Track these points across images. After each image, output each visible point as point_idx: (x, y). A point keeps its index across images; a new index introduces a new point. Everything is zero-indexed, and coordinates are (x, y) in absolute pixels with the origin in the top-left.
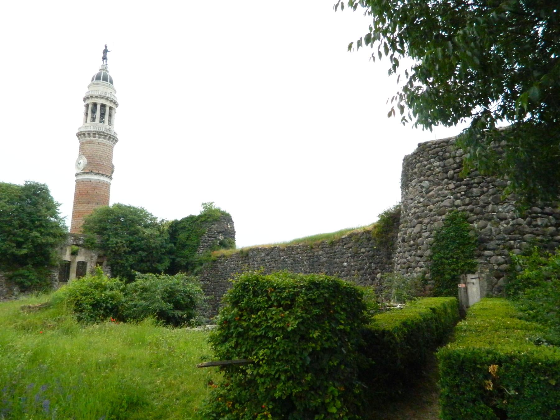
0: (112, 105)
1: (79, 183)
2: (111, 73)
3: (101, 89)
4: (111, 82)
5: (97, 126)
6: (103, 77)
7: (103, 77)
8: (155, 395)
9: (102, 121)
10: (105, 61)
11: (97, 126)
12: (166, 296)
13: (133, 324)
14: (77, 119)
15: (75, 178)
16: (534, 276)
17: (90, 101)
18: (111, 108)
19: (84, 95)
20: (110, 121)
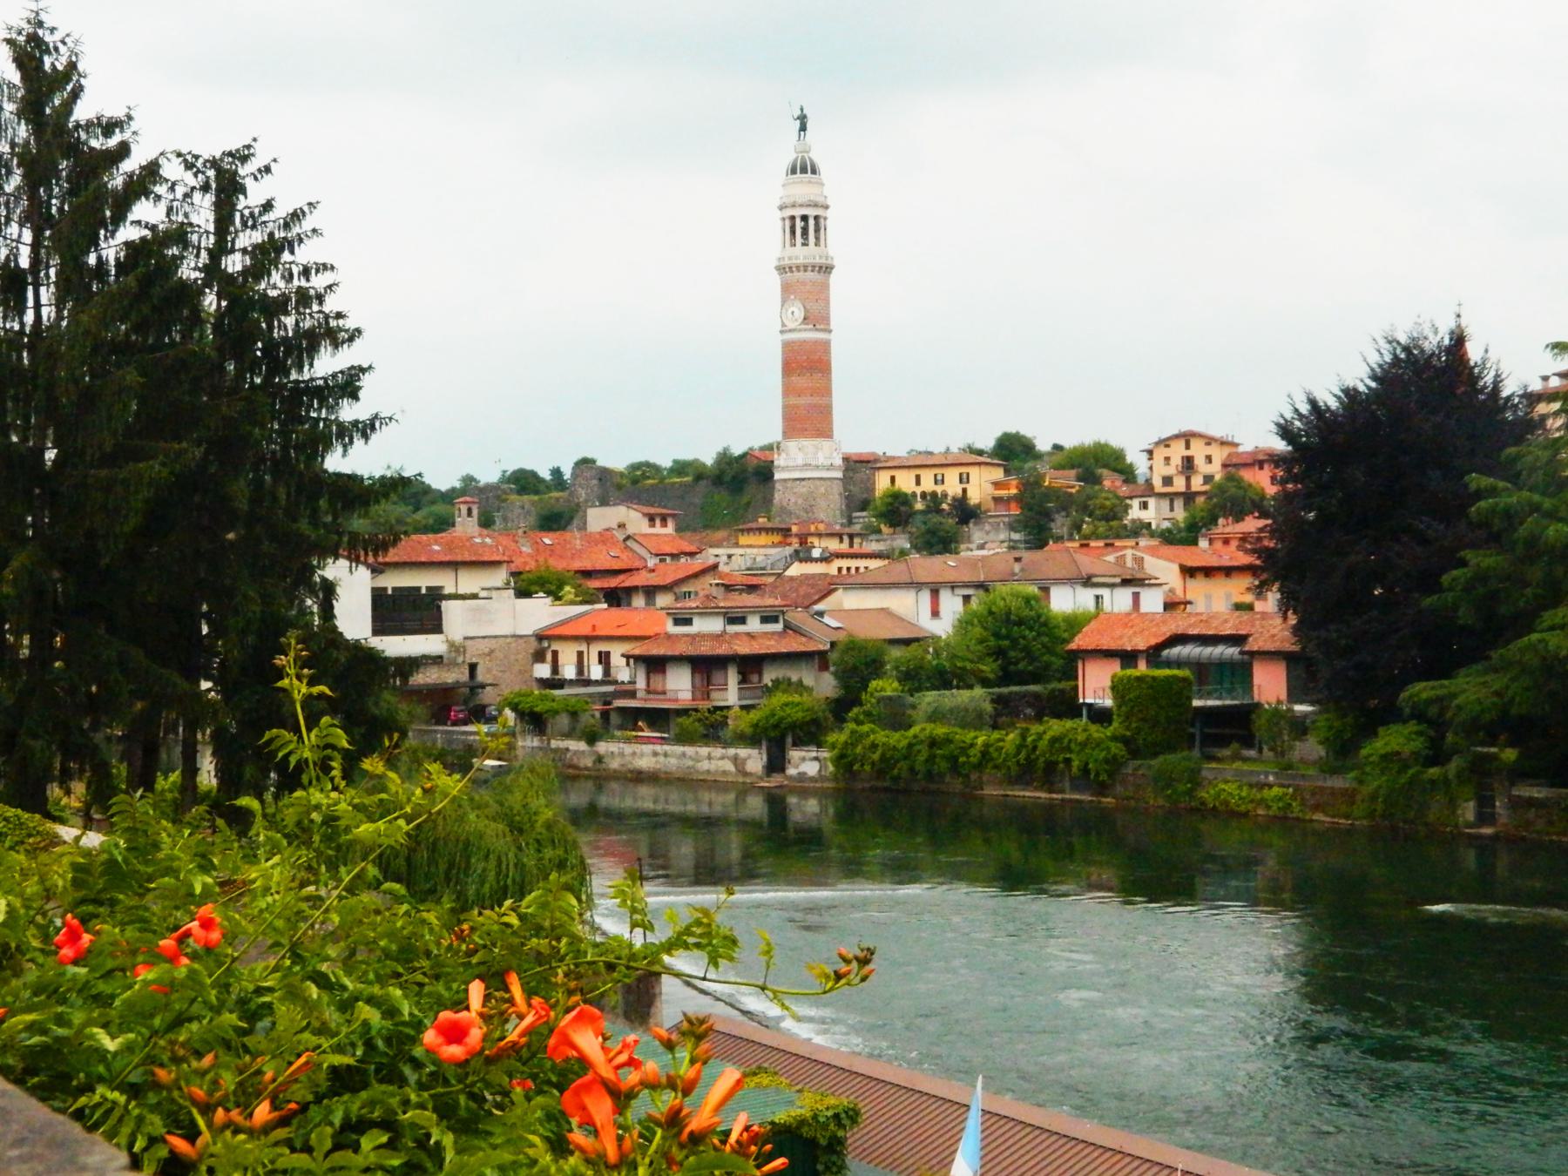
1: (786, 407)
2: (816, 156)
3: (802, 189)
5: (801, 254)
6: (804, 168)
7: (804, 168)
11: (801, 254)
12: (1068, 521)
14: (771, 244)
15: (779, 214)
16: (1221, 521)
17: (789, 212)
18: (816, 218)
19: (778, 203)
20: (817, 238)
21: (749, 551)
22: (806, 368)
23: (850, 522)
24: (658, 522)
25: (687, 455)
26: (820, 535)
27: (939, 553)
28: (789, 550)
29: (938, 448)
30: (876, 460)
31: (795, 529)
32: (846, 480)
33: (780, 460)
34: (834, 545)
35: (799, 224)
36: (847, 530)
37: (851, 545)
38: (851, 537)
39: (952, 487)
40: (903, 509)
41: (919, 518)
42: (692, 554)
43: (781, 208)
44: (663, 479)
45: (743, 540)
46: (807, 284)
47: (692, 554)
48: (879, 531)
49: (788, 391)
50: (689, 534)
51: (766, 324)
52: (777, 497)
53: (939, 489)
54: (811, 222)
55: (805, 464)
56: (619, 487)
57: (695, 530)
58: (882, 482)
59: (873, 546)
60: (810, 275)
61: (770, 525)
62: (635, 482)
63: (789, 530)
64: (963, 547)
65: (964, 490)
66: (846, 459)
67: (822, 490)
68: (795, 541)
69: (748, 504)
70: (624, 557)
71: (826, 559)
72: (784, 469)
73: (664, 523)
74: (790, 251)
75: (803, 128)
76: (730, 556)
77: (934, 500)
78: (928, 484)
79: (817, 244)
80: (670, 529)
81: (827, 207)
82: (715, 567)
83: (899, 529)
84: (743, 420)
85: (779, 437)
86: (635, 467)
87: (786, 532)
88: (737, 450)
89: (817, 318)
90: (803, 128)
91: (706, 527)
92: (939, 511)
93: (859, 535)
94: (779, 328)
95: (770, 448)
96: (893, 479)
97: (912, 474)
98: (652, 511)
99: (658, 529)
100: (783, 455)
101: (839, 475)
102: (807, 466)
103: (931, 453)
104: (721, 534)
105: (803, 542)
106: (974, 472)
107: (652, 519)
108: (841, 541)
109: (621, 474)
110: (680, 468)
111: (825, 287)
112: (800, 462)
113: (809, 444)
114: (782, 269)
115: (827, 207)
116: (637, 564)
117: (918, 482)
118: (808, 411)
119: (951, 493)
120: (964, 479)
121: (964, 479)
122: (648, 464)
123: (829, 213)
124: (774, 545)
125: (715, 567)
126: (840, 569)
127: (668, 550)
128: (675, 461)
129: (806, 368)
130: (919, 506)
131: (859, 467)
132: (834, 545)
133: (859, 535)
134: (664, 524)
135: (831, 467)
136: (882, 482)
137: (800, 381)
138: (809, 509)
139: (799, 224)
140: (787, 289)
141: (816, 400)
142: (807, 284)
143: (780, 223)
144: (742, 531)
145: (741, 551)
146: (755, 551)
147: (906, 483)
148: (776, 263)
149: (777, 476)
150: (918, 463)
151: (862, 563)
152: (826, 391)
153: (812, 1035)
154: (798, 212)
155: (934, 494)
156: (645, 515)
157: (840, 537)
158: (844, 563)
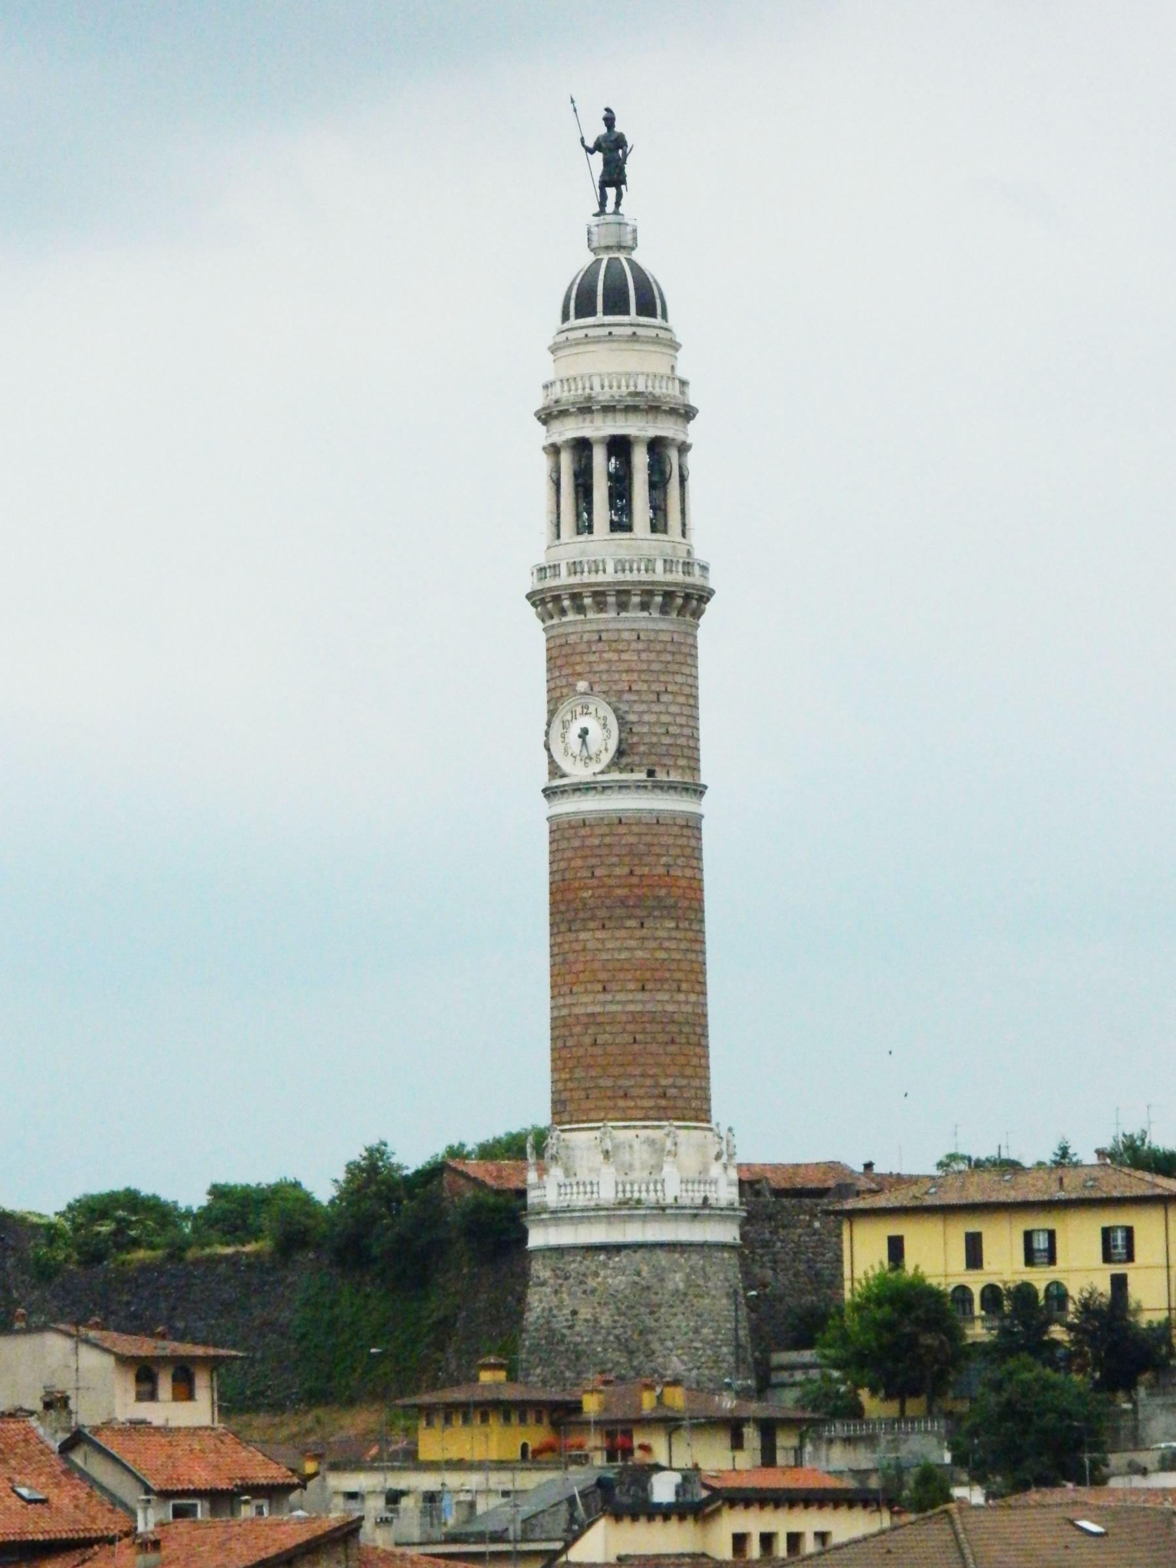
0: (664, 428)
2: (648, 257)
3: (612, 363)
4: (649, 303)
5: (606, 554)
6: (615, 294)
7: (615, 294)
8: (620, 1188)
9: (622, 525)
10: (611, 192)
11: (606, 554)
13: (872, 1268)
14: (515, 520)
15: (541, 436)
17: (571, 429)
20: (659, 510)
21: (453, 1480)
22: (627, 910)
23: (764, 1386)
24: (165, 1386)
25: (254, 1171)
26: (670, 1424)
27: (1046, 1481)
28: (579, 1478)
29: (1033, 1150)
30: (845, 1189)
31: (591, 1405)
32: (748, 1250)
33: (546, 1189)
34: (715, 1459)
35: (601, 464)
36: (754, 1408)
37: (768, 1458)
38: (768, 1429)
39: (1080, 1268)
40: (928, 1340)
41: (978, 1372)
42: (275, 1493)
43: (547, 417)
44: (177, 1251)
45: (433, 1443)
46: (627, 642)
47: (275, 1493)
48: (855, 1412)
49: (565, 974)
50: (261, 1420)
51: (486, 765)
52: (537, 1301)
53: (1040, 1279)
54: (640, 458)
55: (596, 1188)
56: (45, 1272)
57: (277, 1407)
58: (864, 1255)
59: (833, 1462)
60: (635, 618)
61: (512, 1393)
62: (93, 1256)
63: (577, 1407)
64: (1116, 1460)
65: (1119, 1282)
66: (749, 1186)
67: (677, 1280)
68: (594, 1441)
69: (445, 1325)
70: (62, 1499)
71: (695, 1506)
72: (559, 1216)
73: (184, 1391)
74: (574, 546)
75: (613, 177)
76: (394, 1498)
77: (1024, 1310)
78: (1005, 1263)
79: (658, 525)
80: (199, 1411)
81: (687, 414)
82: (349, 1532)
83: (915, 1406)
84: (435, 1058)
85: (543, 1118)
86: (94, 1209)
87: (563, 1414)
88: (411, 1156)
89: (661, 749)
90: (613, 177)
91: (317, 1397)
92: (1045, 1350)
93: (789, 1423)
94: (543, 780)
95: (512, 1148)
96: (896, 1247)
97: (957, 1232)
98: (144, 1347)
99: (165, 1411)
100: (556, 1173)
101: (728, 1233)
102: (627, 1208)
103: (1013, 1166)
104: (356, 1422)
105: (618, 1449)
106: (1148, 1229)
107: (145, 1376)
108: (737, 1443)
109: (50, 1233)
110: (234, 1209)
111: (684, 655)
112: (607, 1194)
113: (633, 1139)
114: (546, 602)
115: (687, 414)
116: (105, 1523)
117: (974, 1259)
118: (633, 1033)
119: (1075, 1289)
120: (1117, 1247)
121: (1117, 1247)
122: (132, 1201)
123: (693, 432)
124: (529, 1458)
125: (349, 1532)
126: (740, 1541)
127: (202, 1478)
128: (218, 1192)
129: (627, 910)
130: (978, 1331)
131: (790, 1211)
132: (715, 1459)
133: (789, 1423)
134: (184, 1391)
135: (703, 1211)
136: (864, 1255)
137: (614, 945)
138: (636, 1344)
139: (601, 464)
140: (562, 660)
141: (661, 1001)
142: (627, 642)
143: (544, 463)
144: (427, 1412)
145: (427, 1481)
146: (473, 1480)
147: (934, 1256)
148: (530, 583)
149: (537, 1238)
150: (976, 1194)
151: (808, 1522)
152: (694, 978)
153: (128, 1257)
154: (599, 429)
155: (1024, 1293)
156: (124, 1361)
157: (734, 1428)
158: (754, 1522)
